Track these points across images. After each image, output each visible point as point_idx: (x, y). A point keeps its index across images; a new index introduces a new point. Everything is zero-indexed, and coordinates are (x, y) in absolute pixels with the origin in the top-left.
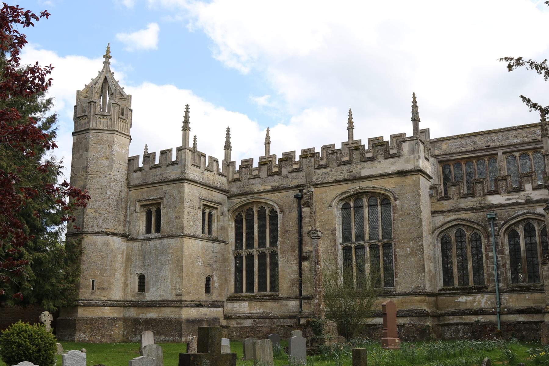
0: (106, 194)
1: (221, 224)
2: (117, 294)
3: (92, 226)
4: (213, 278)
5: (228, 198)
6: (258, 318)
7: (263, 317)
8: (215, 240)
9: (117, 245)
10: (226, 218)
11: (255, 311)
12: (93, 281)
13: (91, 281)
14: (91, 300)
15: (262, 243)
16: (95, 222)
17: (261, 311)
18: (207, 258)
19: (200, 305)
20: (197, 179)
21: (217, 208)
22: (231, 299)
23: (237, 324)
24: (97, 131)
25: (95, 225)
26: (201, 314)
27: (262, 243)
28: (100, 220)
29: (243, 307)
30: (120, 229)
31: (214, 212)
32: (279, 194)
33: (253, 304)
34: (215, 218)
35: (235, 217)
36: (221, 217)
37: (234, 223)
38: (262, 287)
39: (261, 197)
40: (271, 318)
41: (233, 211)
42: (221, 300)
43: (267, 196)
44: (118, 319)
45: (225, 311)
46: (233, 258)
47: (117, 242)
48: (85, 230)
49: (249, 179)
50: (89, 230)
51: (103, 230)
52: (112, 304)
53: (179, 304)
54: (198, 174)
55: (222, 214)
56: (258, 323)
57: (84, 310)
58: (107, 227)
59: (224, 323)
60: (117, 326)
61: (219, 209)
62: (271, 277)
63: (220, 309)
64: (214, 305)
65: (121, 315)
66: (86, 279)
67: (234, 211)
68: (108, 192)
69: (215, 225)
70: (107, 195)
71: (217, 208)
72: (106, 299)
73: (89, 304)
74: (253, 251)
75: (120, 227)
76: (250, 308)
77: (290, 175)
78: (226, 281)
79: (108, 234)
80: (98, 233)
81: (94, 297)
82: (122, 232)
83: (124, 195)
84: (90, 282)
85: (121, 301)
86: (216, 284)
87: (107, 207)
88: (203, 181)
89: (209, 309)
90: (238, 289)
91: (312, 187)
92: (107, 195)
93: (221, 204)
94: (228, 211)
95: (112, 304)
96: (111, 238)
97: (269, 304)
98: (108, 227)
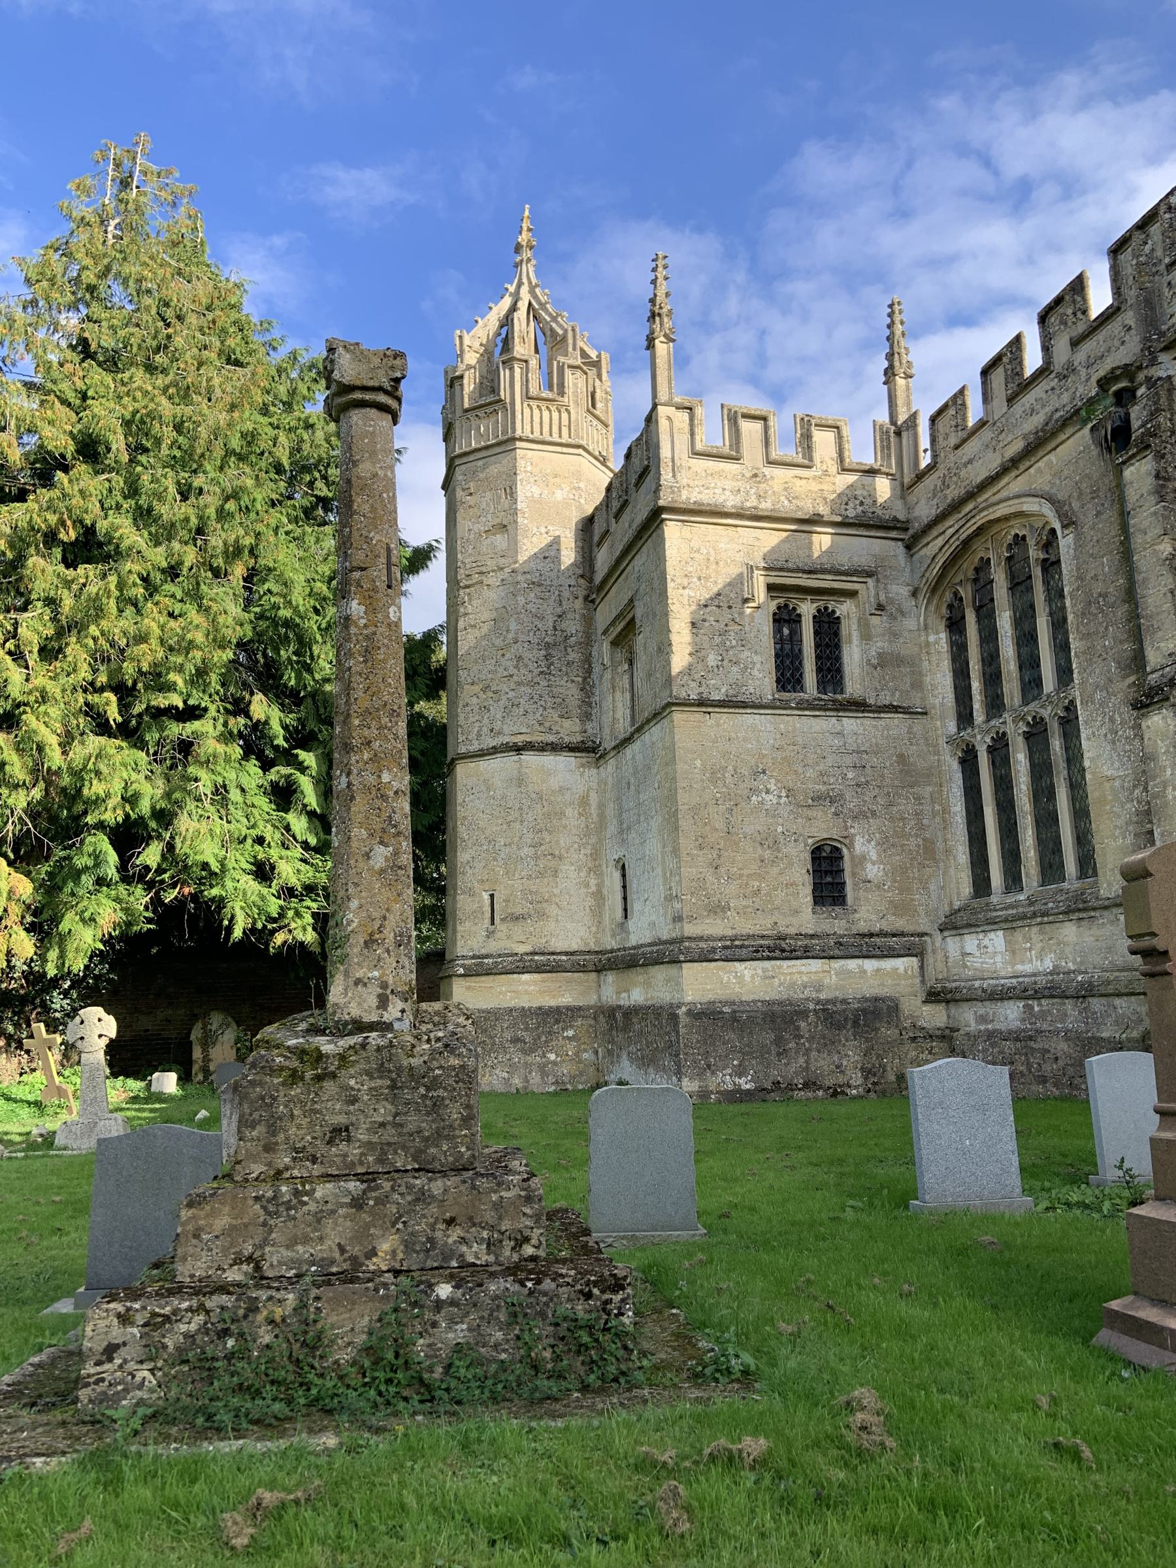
0: (508, 631)
1: (880, 644)
2: (570, 932)
3: (479, 735)
4: (850, 847)
5: (908, 547)
6: (1038, 995)
7: (1049, 990)
8: (858, 706)
9: (554, 783)
10: (910, 623)
11: (1028, 968)
12: (492, 896)
13: (486, 896)
14: (487, 956)
15: (1031, 685)
16: (486, 721)
17: (1048, 964)
18: (810, 773)
19: (779, 948)
20: (730, 502)
21: (853, 594)
22: (953, 924)
23: (982, 1019)
24: (471, 458)
25: (485, 729)
26: (792, 985)
27: (1031, 685)
28: (497, 711)
29: (988, 954)
30: (570, 730)
31: (844, 609)
32: (1052, 457)
33: (1018, 936)
34: (850, 630)
35: (944, 610)
36: (875, 620)
37: (943, 635)
38: (1051, 868)
39: (1004, 494)
40: (1085, 993)
41: (934, 591)
42: (909, 928)
43: (1014, 484)
44: (573, 1012)
45: (930, 972)
46: (955, 765)
47: (561, 770)
48: (462, 749)
49: (957, 447)
50: (471, 748)
51: (506, 739)
52: (543, 963)
53: (668, 954)
54: (729, 484)
55: (880, 607)
56: (1043, 1015)
57: (468, 988)
58: (515, 729)
59: (934, 1017)
60: (570, 1033)
61: (862, 593)
62: (1054, 818)
63: (902, 964)
64: (869, 945)
65: (592, 999)
66: (471, 893)
67: (935, 588)
68: (513, 626)
69: (853, 657)
70: (510, 636)
71: (853, 594)
72: (527, 948)
73: (482, 969)
74: (1004, 723)
75: (567, 723)
76: (1012, 950)
77: (1081, 355)
78: (929, 852)
79: (518, 749)
80: (494, 751)
81: (493, 947)
82: (577, 739)
83: (572, 626)
84: (481, 901)
85: (583, 953)
86: (873, 871)
87: (512, 670)
88: (763, 506)
89: (837, 964)
90: (981, 885)
91: (1163, 357)
92: (510, 636)
93: (870, 574)
94: (914, 594)
95: (543, 963)
96: (529, 758)
97: (1069, 931)
98: (515, 729)
